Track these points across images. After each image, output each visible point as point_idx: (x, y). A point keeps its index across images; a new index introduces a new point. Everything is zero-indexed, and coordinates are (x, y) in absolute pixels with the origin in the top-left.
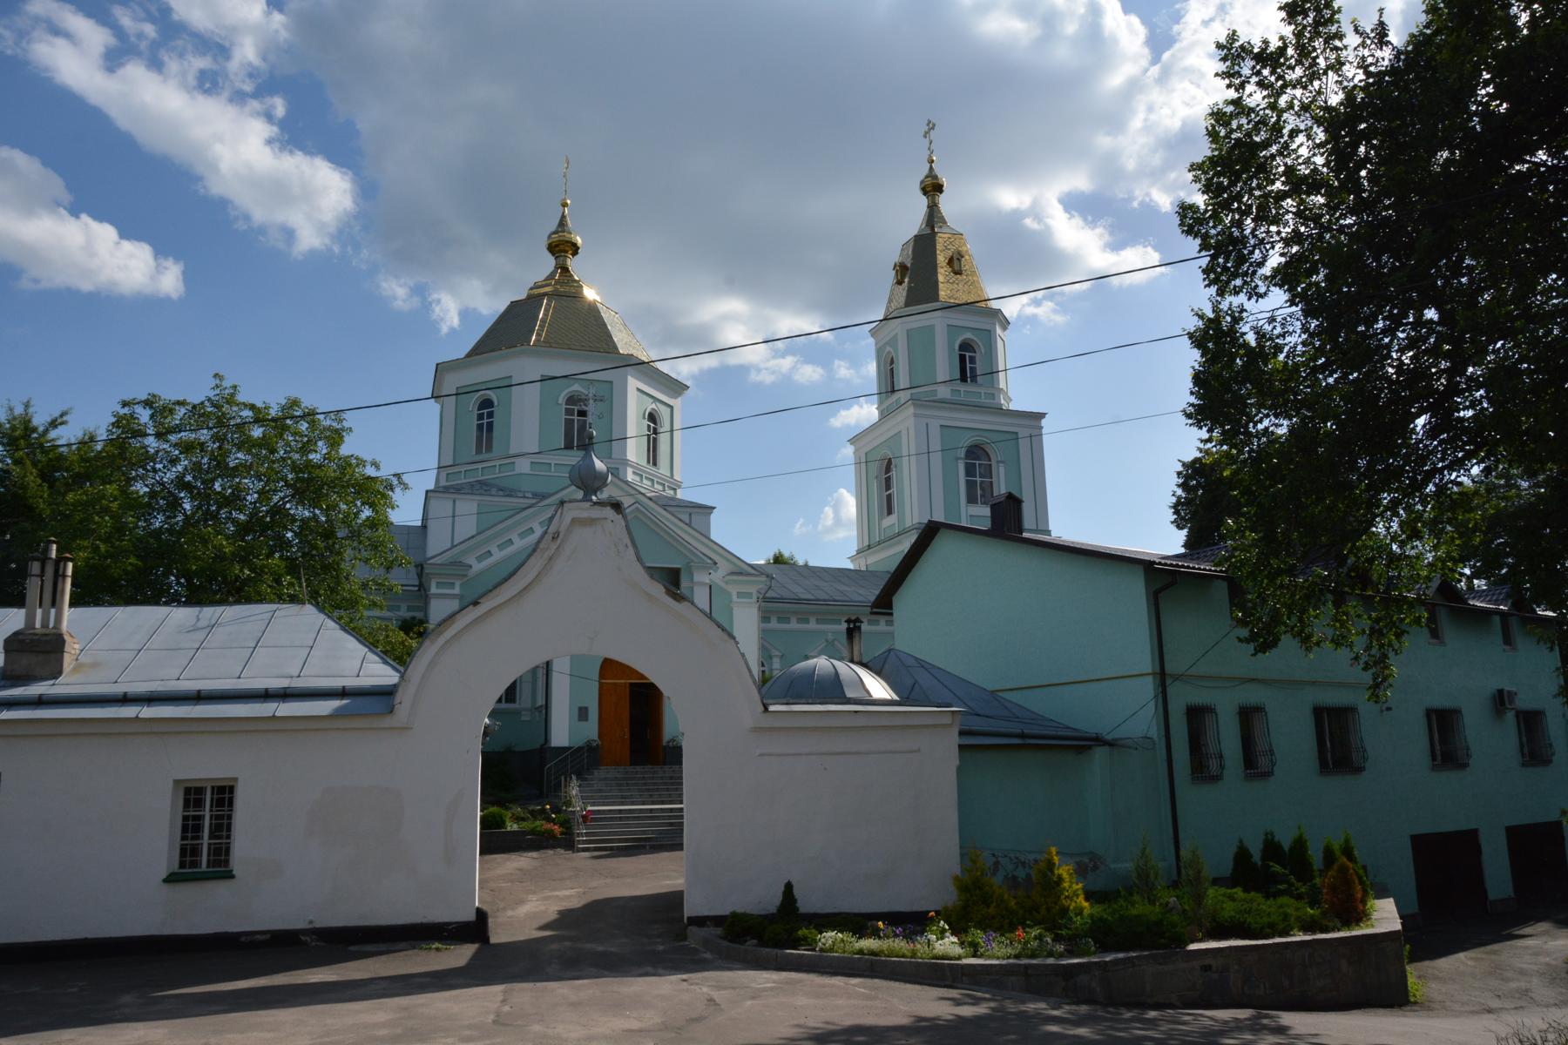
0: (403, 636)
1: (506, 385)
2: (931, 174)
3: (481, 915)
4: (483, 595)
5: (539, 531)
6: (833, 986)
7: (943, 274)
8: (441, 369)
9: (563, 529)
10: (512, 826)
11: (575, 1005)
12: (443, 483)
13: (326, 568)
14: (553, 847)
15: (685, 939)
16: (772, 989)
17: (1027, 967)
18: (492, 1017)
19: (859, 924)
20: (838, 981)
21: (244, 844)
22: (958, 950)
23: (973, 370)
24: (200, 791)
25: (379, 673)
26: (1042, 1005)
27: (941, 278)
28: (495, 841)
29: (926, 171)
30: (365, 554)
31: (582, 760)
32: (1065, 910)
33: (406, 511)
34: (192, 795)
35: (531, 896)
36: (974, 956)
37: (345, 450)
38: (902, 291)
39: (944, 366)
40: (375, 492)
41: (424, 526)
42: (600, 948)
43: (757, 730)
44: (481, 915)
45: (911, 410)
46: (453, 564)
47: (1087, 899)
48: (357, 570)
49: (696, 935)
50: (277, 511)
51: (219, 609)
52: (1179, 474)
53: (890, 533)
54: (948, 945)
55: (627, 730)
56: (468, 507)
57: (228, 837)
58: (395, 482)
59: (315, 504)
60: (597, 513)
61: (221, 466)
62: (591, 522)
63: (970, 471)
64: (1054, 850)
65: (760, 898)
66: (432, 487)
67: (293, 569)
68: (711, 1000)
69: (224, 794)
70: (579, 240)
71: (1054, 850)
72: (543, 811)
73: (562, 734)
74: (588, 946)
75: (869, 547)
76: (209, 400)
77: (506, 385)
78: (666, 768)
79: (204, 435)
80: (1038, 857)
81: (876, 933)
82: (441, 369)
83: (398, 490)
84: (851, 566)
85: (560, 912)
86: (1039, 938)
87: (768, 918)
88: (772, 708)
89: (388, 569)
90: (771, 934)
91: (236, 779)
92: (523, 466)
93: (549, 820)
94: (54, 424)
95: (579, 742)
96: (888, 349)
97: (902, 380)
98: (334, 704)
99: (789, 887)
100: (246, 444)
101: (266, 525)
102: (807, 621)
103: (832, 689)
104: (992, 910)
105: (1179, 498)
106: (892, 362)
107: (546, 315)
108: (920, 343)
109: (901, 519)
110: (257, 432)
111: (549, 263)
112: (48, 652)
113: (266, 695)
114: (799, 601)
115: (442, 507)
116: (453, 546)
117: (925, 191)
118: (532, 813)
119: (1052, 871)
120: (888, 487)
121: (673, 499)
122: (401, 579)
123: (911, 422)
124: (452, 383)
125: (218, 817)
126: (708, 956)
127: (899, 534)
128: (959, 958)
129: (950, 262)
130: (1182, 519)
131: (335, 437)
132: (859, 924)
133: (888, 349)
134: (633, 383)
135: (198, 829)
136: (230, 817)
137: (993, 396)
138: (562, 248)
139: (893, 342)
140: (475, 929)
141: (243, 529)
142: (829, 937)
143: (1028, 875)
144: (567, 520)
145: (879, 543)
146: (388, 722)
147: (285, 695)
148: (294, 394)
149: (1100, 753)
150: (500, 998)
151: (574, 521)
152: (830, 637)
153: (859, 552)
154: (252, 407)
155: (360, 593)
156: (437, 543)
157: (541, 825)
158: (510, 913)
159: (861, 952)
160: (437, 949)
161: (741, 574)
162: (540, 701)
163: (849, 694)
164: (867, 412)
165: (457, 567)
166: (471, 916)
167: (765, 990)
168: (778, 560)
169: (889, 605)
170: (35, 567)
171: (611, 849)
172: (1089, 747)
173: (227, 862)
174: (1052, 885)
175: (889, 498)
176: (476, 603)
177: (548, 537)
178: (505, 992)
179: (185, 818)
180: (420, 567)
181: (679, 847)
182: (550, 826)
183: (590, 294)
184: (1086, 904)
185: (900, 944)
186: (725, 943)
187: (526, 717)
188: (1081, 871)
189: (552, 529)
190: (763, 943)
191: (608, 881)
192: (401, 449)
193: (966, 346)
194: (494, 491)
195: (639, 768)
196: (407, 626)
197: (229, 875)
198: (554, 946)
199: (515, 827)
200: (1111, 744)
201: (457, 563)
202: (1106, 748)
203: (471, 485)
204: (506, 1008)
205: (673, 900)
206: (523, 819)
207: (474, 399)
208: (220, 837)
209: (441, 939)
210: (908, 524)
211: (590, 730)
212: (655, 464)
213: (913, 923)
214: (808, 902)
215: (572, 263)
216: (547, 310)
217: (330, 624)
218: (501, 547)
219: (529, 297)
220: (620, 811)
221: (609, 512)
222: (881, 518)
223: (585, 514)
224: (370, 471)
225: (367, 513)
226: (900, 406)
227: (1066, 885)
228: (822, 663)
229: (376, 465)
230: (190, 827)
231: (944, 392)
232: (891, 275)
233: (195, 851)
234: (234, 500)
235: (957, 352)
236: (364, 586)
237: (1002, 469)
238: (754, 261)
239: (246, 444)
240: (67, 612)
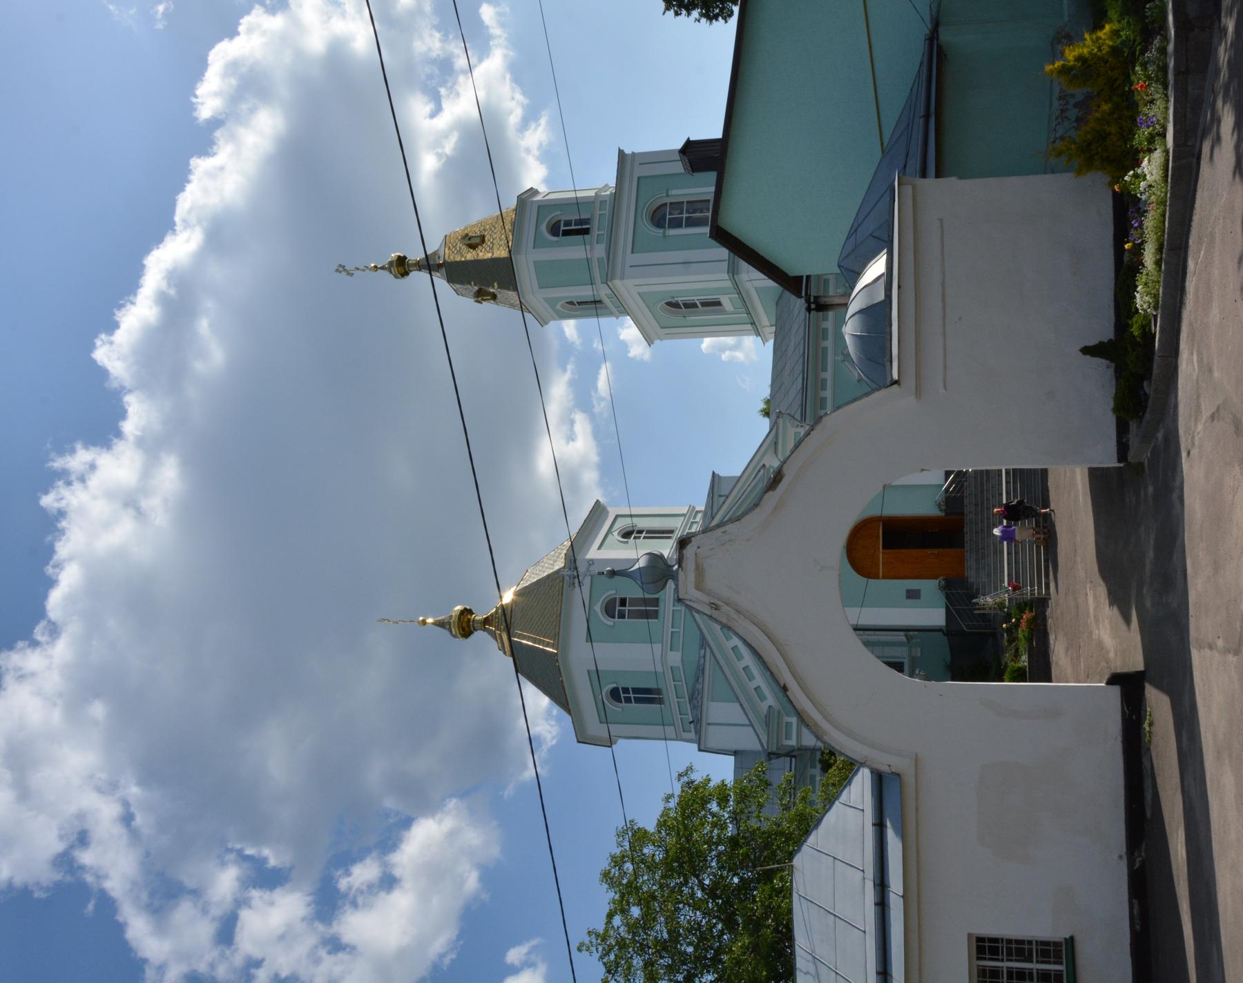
0: (832, 767)
1: (596, 675)
2: (389, 268)
3: (1114, 679)
4: (777, 682)
5: (735, 641)
6: (1197, 289)
7: (483, 254)
8: (583, 738)
9: (707, 599)
10: (1024, 660)
11: (1217, 567)
12: (692, 735)
13: (767, 846)
14: (1045, 619)
15: (1141, 464)
16: (1200, 354)
17: (1177, 73)
18: (1231, 658)
19: (1126, 271)
20: (1191, 285)
22: (1158, 155)
23: (580, 222)
25: (860, 789)
26: (1222, 49)
27: (489, 255)
28: (1041, 669)
29: (386, 273)
30: (754, 808)
31: (959, 594)
32: (1115, 51)
33: (720, 770)
35: (1095, 633)
36: (1164, 135)
37: (651, 827)
38: (504, 294)
39: (572, 251)
40: (695, 797)
41: (735, 753)
42: (1151, 554)
43: (918, 392)
44: (1114, 679)
45: (617, 282)
46: (767, 725)
47: (1102, 27)
48: (770, 815)
49: (1139, 453)
50: (711, 892)
51: (798, 951)
52: (677, 14)
53: (739, 303)
54: (1151, 168)
55: (929, 551)
56: (719, 711)
57: (1030, 942)
58: (685, 779)
59: (703, 857)
60: (690, 564)
61: (664, 947)
62: (699, 570)
63: (676, 224)
64: (1048, 68)
65: (1096, 384)
66: (695, 746)
67: (768, 876)
68: (1212, 417)
70: (459, 608)
71: (1048, 68)
72: (1008, 630)
73: (935, 616)
74: (1148, 566)
75: (753, 323)
76: (601, 958)
77: (596, 675)
78: (966, 510)
79: (638, 962)
80: (1057, 90)
81: (1138, 250)
82: (583, 738)
83: (693, 776)
84: (772, 342)
85: (1111, 604)
86: (1144, 66)
87: (1119, 373)
88: (895, 376)
89: (768, 784)
90: (1137, 367)
91: (970, 935)
92: (675, 658)
93: (1017, 625)
95: (941, 598)
96: (558, 307)
97: (585, 293)
98: (890, 834)
99: (1086, 351)
100: (647, 921)
101: (727, 903)
102: (824, 381)
103: (876, 315)
104: (1113, 129)
105: (702, 15)
106: (571, 303)
107: (528, 639)
108: (549, 275)
109: (724, 291)
110: (636, 912)
111: (479, 636)
113: (882, 904)
114: (804, 389)
115: (714, 736)
116: (751, 725)
117: (405, 274)
118: (1010, 642)
119: (1071, 69)
120: (694, 305)
121: (705, 513)
122: (781, 773)
123: (630, 283)
124: (595, 727)
125: (1009, 953)
126: (1160, 435)
127: (740, 293)
128: (1167, 152)
129: (473, 247)
130: (722, 10)
131: (639, 837)
132: (1126, 271)
133: (558, 307)
134: (593, 553)
136: (1009, 941)
137: (603, 202)
138: (465, 625)
139: (552, 302)
140: (1130, 686)
141: (730, 925)
142: (1141, 300)
143: (1076, 105)
145: (749, 313)
146: (909, 780)
147: (882, 885)
148: (597, 876)
149: (945, 36)
150: (1208, 652)
151: (698, 588)
152: (839, 358)
153: (758, 334)
154: (610, 916)
155: (793, 811)
156: (749, 740)
157: (1021, 633)
158: (1112, 655)
159: (1158, 263)
160: (1151, 725)
161: (776, 444)
162: (901, 637)
163: (881, 297)
164: (629, 331)
165: (770, 720)
166: (1116, 690)
167: (1200, 361)
168: (766, 413)
171: (1046, 561)
172: (939, 47)
173: (1057, 944)
174: (1086, 69)
175: (704, 304)
176: (785, 689)
177: (715, 614)
178: (1200, 648)
180: (771, 755)
181: (1044, 472)
182: (1023, 624)
183: (508, 597)
184: (1107, 27)
185: (1150, 222)
186: (1147, 416)
187: (917, 652)
188: (1070, 38)
189: (708, 611)
190: (1146, 374)
191: (1079, 559)
192: (654, 773)
193: (555, 230)
194: (700, 686)
195: (967, 538)
196: (826, 766)
197: (1071, 941)
198: (1148, 604)
199: (1025, 658)
200: (936, 25)
202: (941, 29)
203: (694, 708)
204: (1220, 643)
205: (1097, 477)
206: (1017, 650)
207: (611, 706)
208: (1030, 951)
210: (729, 284)
211: (930, 587)
212: (672, 532)
213: (1126, 209)
214: (1104, 331)
215: (479, 617)
216: (524, 638)
218: (751, 678)
219: (513, 655)
220: (1009, 554)
221: (689, 551)
222: (724, 312)
223: (692, 577)
224: (673, 804)
225: (714, 807)
226: (615, 295)
227: (1086, 51)
228: (850, 329)
229: (668, 798)
231: (600, 251)
232: (488, 306)
234: (703, 937)
235: (561, 238)
236: (787, 808)
237: (674, 192)
238: (482, 443)
239: (647, 921)
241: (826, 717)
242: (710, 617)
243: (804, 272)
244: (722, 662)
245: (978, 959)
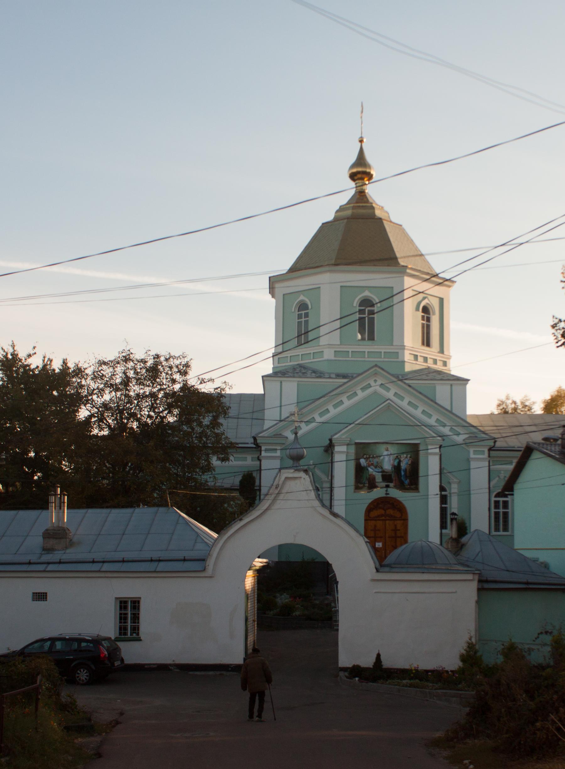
21: (146, 625)
24: (126, 602)
34: (123, 604)
56: (291, 387)
57: (138, 623)
69: (136, 603)
91: (140, 598)
94: (29, 356)
99: (379, 656)
112: (60, 538)
115: (275, 385)
125: (134, 614)
135: (126, 618)
136: (139, 614)
144: (283, 478)
169: (512, 489)
170: (52, 499)
177: (274, 487)
179: (121, 614)
197: (139, 640)
201: (278, 435)
203: (294, 368)
208: (135, 623)
230: (123, 618)
233: (125, 629)
241: (229, 538)
242: (272, 485)
243: (516, 492)
244: (318, 403)
245: (131, 601)
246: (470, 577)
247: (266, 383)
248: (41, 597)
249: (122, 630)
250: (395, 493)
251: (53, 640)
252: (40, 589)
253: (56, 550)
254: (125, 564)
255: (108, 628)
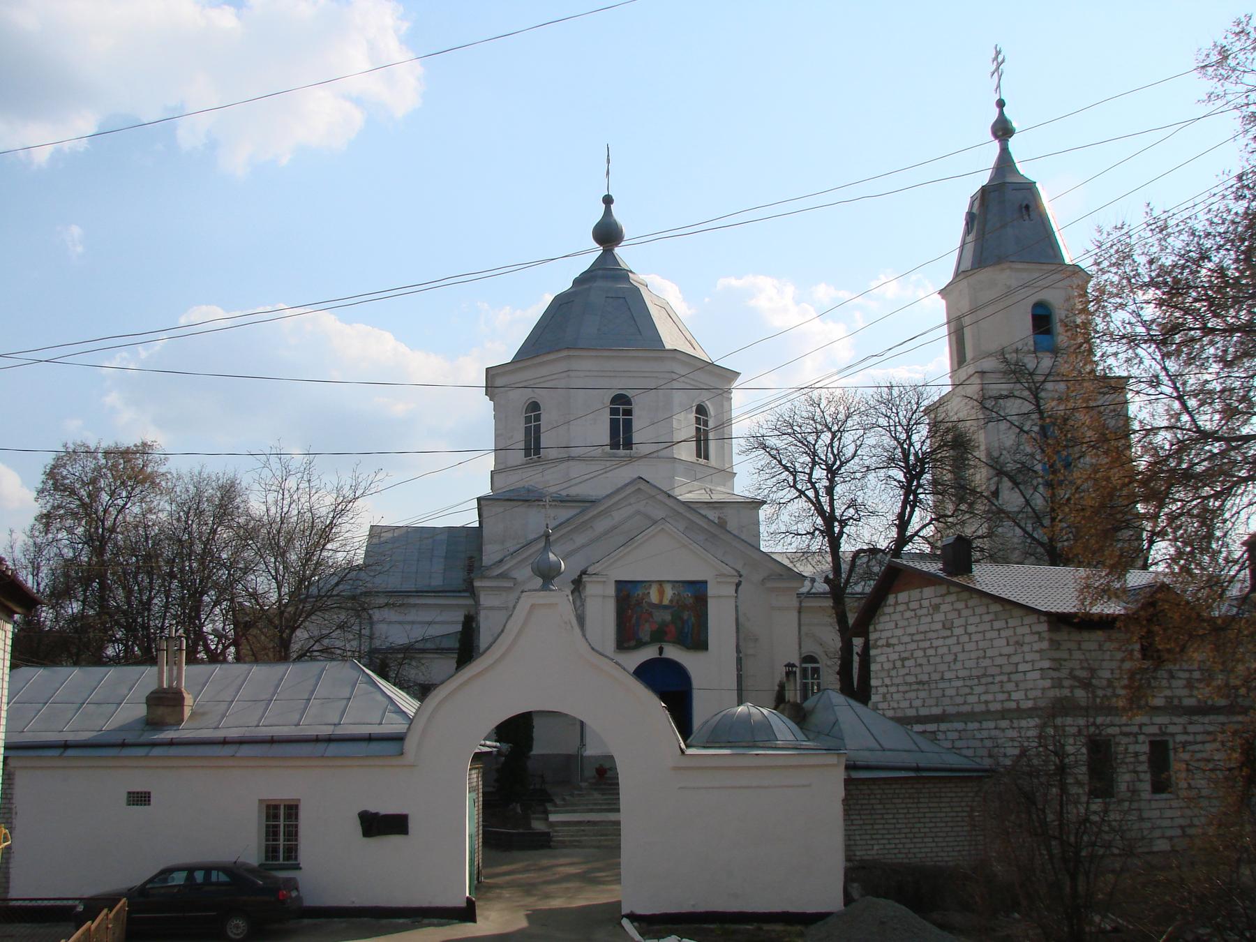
24: (276, 807)
43: (676, 769)
66: (486, 490)
69: (292, 810)
97: (969, 354)
111: (598, 250)
125: (289, 826)
135: (276, 834)
151: (533, 606)
179: (267, 826)
209: (441, 917)
212: (707, 458)
217: (489, 462)
230: (272, 832)
240: (184, 667)
246: (832, 759)
247: (485, 509)
248: (140, 798)
249: (271, 852)
250: (673, 653)
251: (208, 869)
252: (138, 788)
253: (167, 724)
254: (275, 746)
255: (245, 846)
